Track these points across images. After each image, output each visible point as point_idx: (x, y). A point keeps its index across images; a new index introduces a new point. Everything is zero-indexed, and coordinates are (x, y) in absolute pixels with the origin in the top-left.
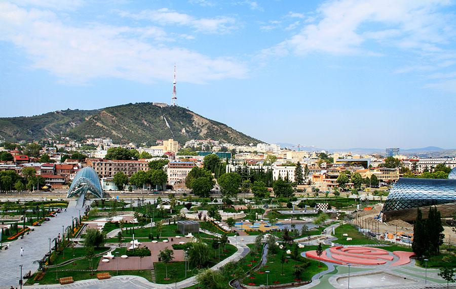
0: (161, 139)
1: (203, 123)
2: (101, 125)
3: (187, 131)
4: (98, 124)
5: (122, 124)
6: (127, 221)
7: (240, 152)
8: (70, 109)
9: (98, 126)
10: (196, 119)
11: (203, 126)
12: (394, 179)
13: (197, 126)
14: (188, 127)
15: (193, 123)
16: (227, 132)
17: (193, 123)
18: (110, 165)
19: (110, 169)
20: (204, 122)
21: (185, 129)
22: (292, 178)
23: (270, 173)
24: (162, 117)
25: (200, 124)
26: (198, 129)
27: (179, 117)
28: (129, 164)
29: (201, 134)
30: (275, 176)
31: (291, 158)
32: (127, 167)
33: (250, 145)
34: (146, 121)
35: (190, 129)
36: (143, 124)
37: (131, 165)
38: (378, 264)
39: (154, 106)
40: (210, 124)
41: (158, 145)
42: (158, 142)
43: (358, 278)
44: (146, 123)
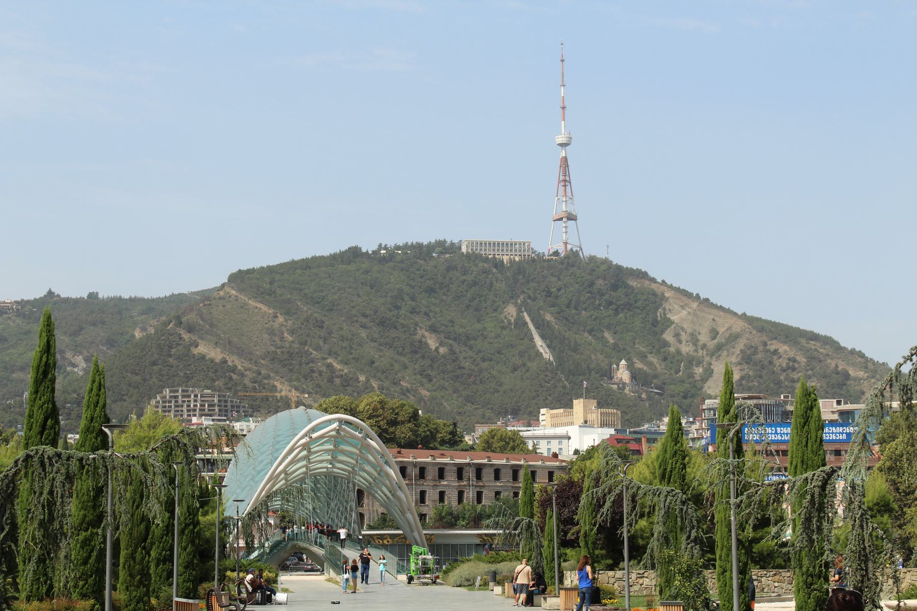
1: (714, 333)
2: (216, 354)
4: (202, 349)
5: (318, 348)
8: (56, 291)
9: (203, 357)
10: (677, 315)
11: (719, 348)
13: (686, 349)
14: (643, 357)
15: (668, 336)
16: (847, 376)
17: (668, 336)
20: (721, 330)
21: (630, 367)
22: (691, 436)
24: (511, 311)
25: (704, 338)
26: (691, 361)
27: (597, 308)
34: (433, 329)
35: (650, 364)
36: (419, 348)
38: (238, 511)
39: (468, 256)
40: (757, 339)
43: (564, 600)
44: (432, 343)
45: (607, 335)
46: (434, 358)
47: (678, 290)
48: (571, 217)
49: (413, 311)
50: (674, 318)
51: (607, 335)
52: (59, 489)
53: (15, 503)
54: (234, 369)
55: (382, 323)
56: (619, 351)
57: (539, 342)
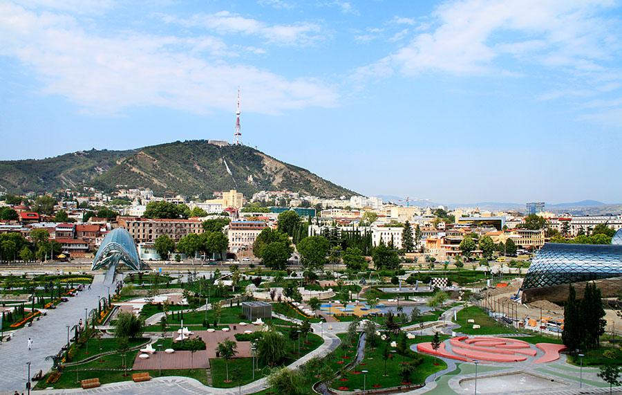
0: (219, 190)
1: (276, 168)
2: (138, 171)
3: (255, 179)
4: (134, 169)
5: (166, 170)
6: (173, 302)
7: (327, 208)
8: (95, 148)
9: (133, 172)
11: (277, 172)
12: (538, 245)
13: (268, 172)
14: (256, 174)
15: (264, 168)
16: (310, 181)
17: (264, 168)
18: (151, 225)
19: (150, 231)
21: (253, 177)
23: (369, 237)
24: (221, 160)
26: (270, 176)
28: (176, 224)
29: (274, 183)
30: (376, 240)
31: (397, 217)
32: (174, 228)
33: (341, 198)
34: (199, 165)
35: (259, 176)
37: (179, 225)
39: (210, 145)
40: (287, 170)
41: (215, 198)
42: (215, 194)
44: (199, 169)
45: (247, 167)
46: (199, 173)
47: (267, 156)
48: (239, 134)
49: (194, 160)
50: (266, 164)
51: (247, 167)
52: (96, 205)
53: (568, 295)
54: (142, 175)
55: (185, 163)
56: (250, 172)
57: (228, 169)
